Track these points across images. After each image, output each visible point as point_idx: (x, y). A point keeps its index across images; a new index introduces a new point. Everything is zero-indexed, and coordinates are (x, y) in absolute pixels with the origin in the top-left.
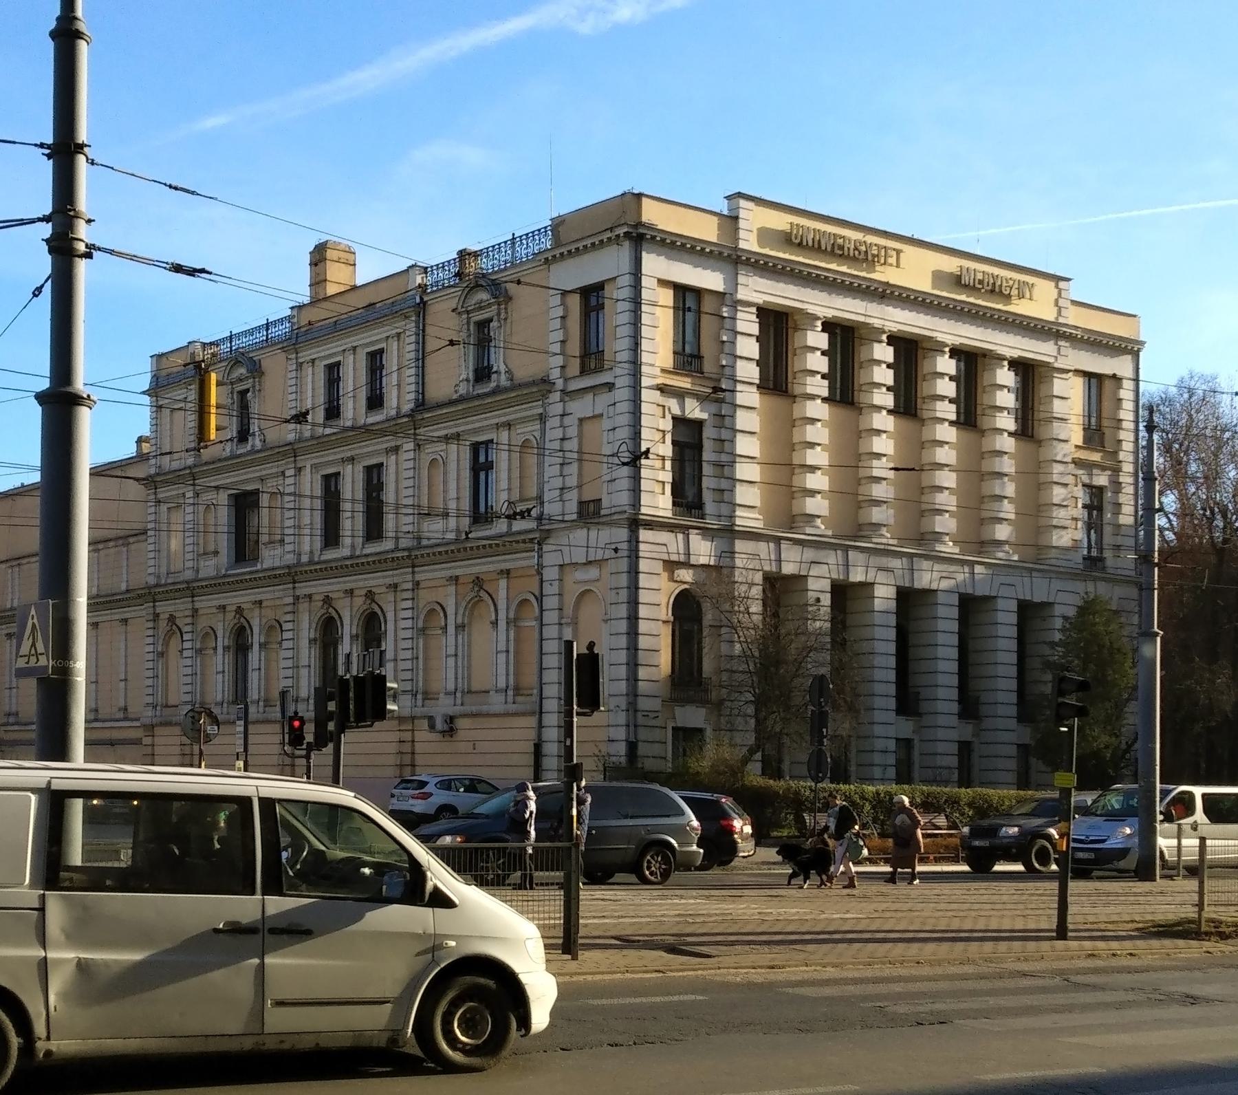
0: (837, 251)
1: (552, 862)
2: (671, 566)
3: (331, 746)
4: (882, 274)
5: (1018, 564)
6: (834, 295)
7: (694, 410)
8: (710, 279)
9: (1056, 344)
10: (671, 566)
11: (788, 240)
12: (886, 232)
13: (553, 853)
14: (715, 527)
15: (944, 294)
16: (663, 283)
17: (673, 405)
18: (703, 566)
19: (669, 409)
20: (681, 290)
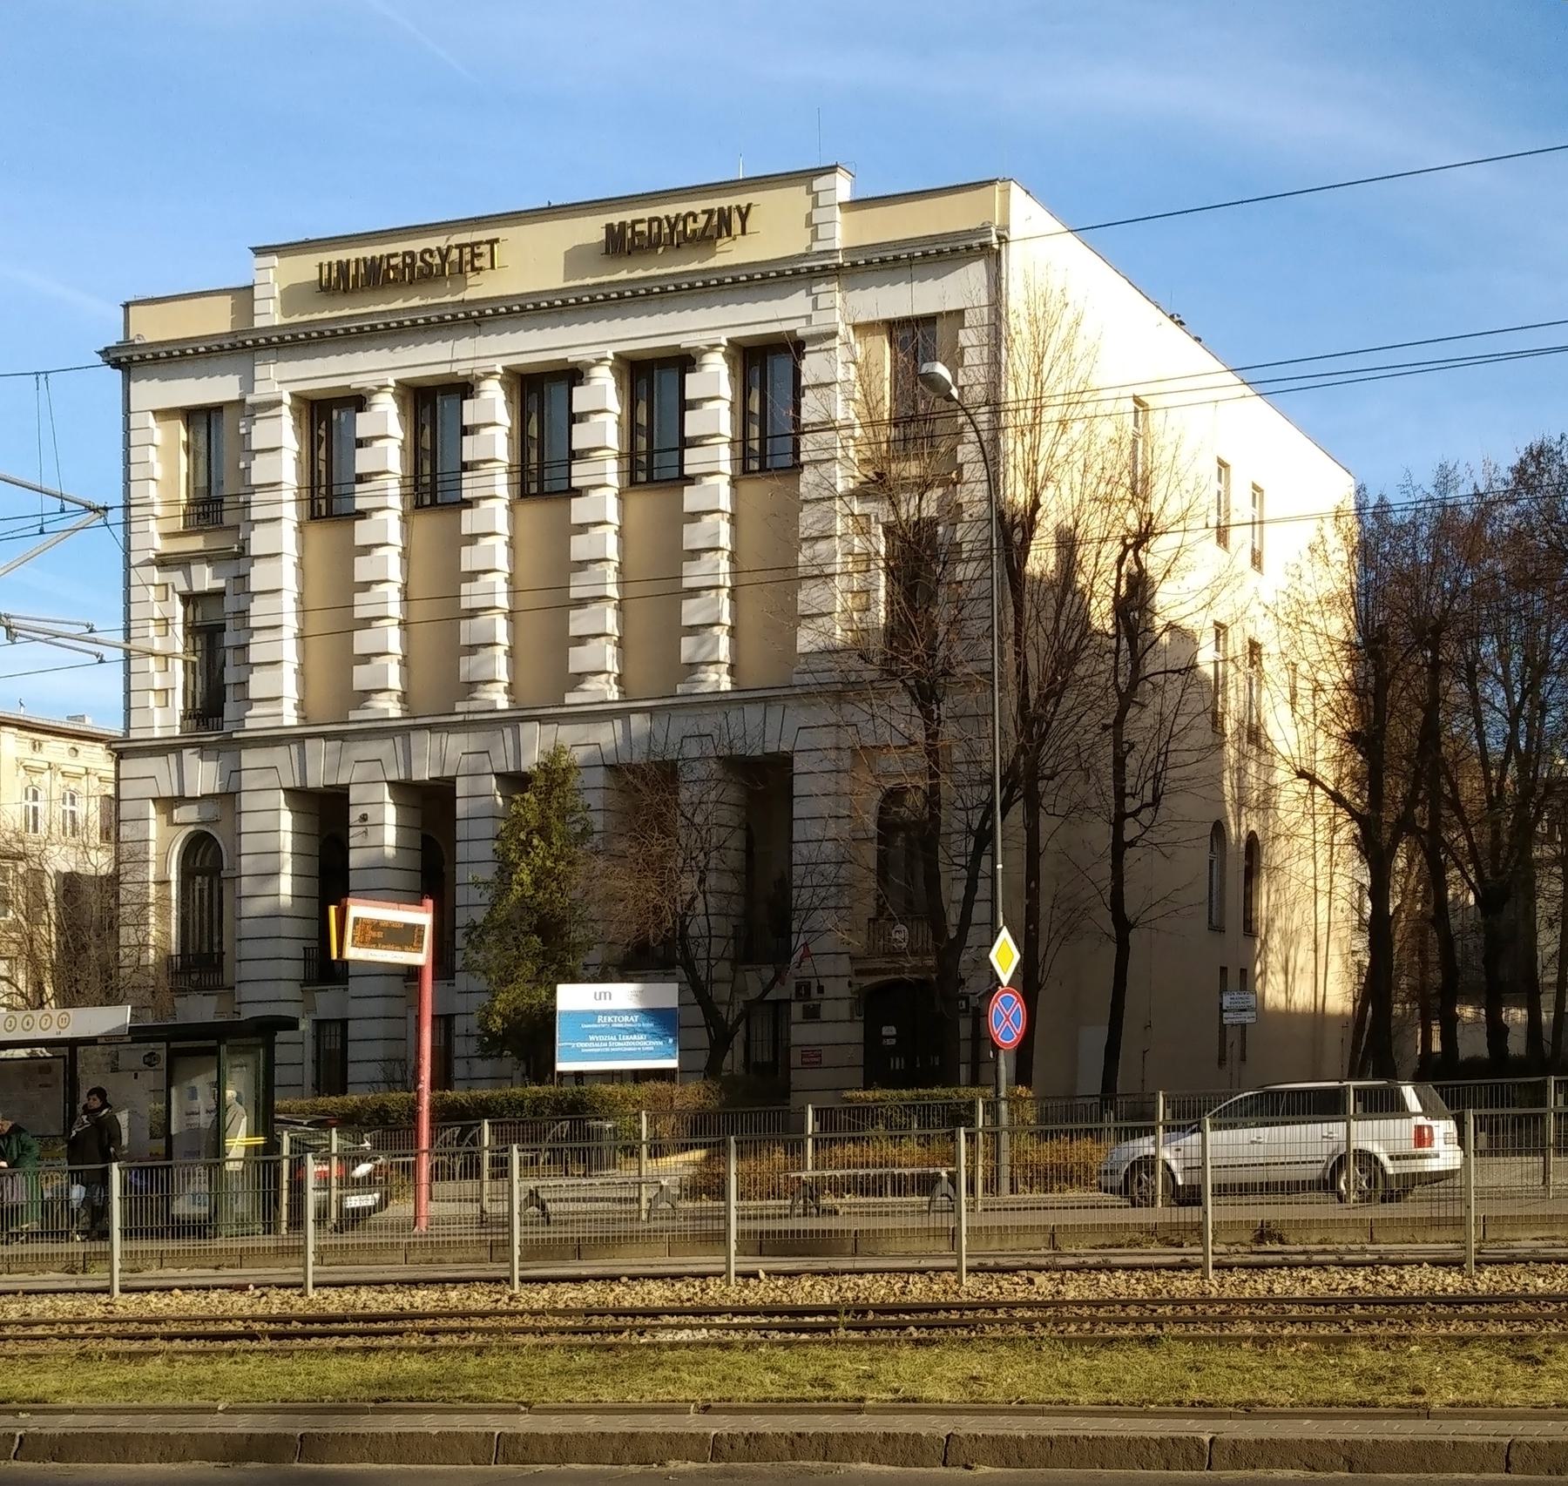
0: (419, 274)
1: (1502, 1095)
2: (167, 804)
3: (768, 997)
4: (480, 288)
5: (731, 696)
6: (399, 349)
7: (205, 579)
8: (218, 388)
9: (809, 294)
10: (167, 804)
11: (337, 284)
12: (307, 242)
13: (1497, 1089)
14: (214, 739)
15: (589, 281)
16: (162, 414)
17: (177, 579)
18: (203, 797)
19: (173, 587)
20: (194, 416)
